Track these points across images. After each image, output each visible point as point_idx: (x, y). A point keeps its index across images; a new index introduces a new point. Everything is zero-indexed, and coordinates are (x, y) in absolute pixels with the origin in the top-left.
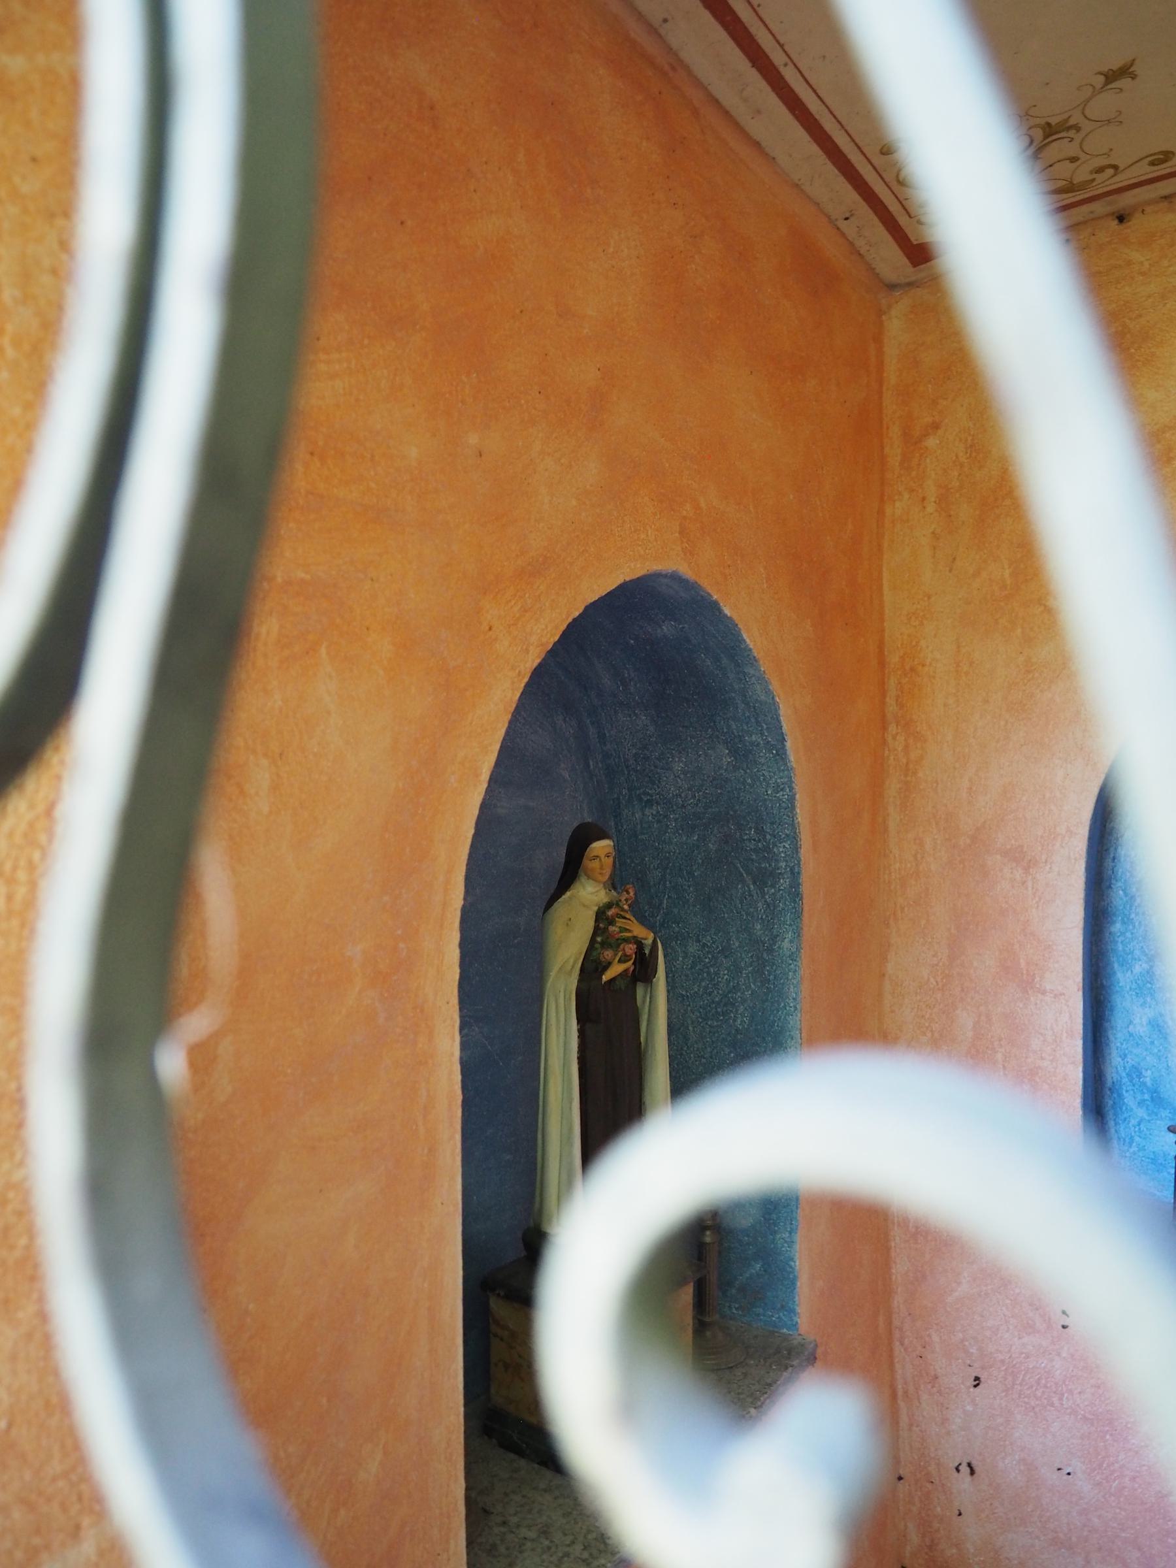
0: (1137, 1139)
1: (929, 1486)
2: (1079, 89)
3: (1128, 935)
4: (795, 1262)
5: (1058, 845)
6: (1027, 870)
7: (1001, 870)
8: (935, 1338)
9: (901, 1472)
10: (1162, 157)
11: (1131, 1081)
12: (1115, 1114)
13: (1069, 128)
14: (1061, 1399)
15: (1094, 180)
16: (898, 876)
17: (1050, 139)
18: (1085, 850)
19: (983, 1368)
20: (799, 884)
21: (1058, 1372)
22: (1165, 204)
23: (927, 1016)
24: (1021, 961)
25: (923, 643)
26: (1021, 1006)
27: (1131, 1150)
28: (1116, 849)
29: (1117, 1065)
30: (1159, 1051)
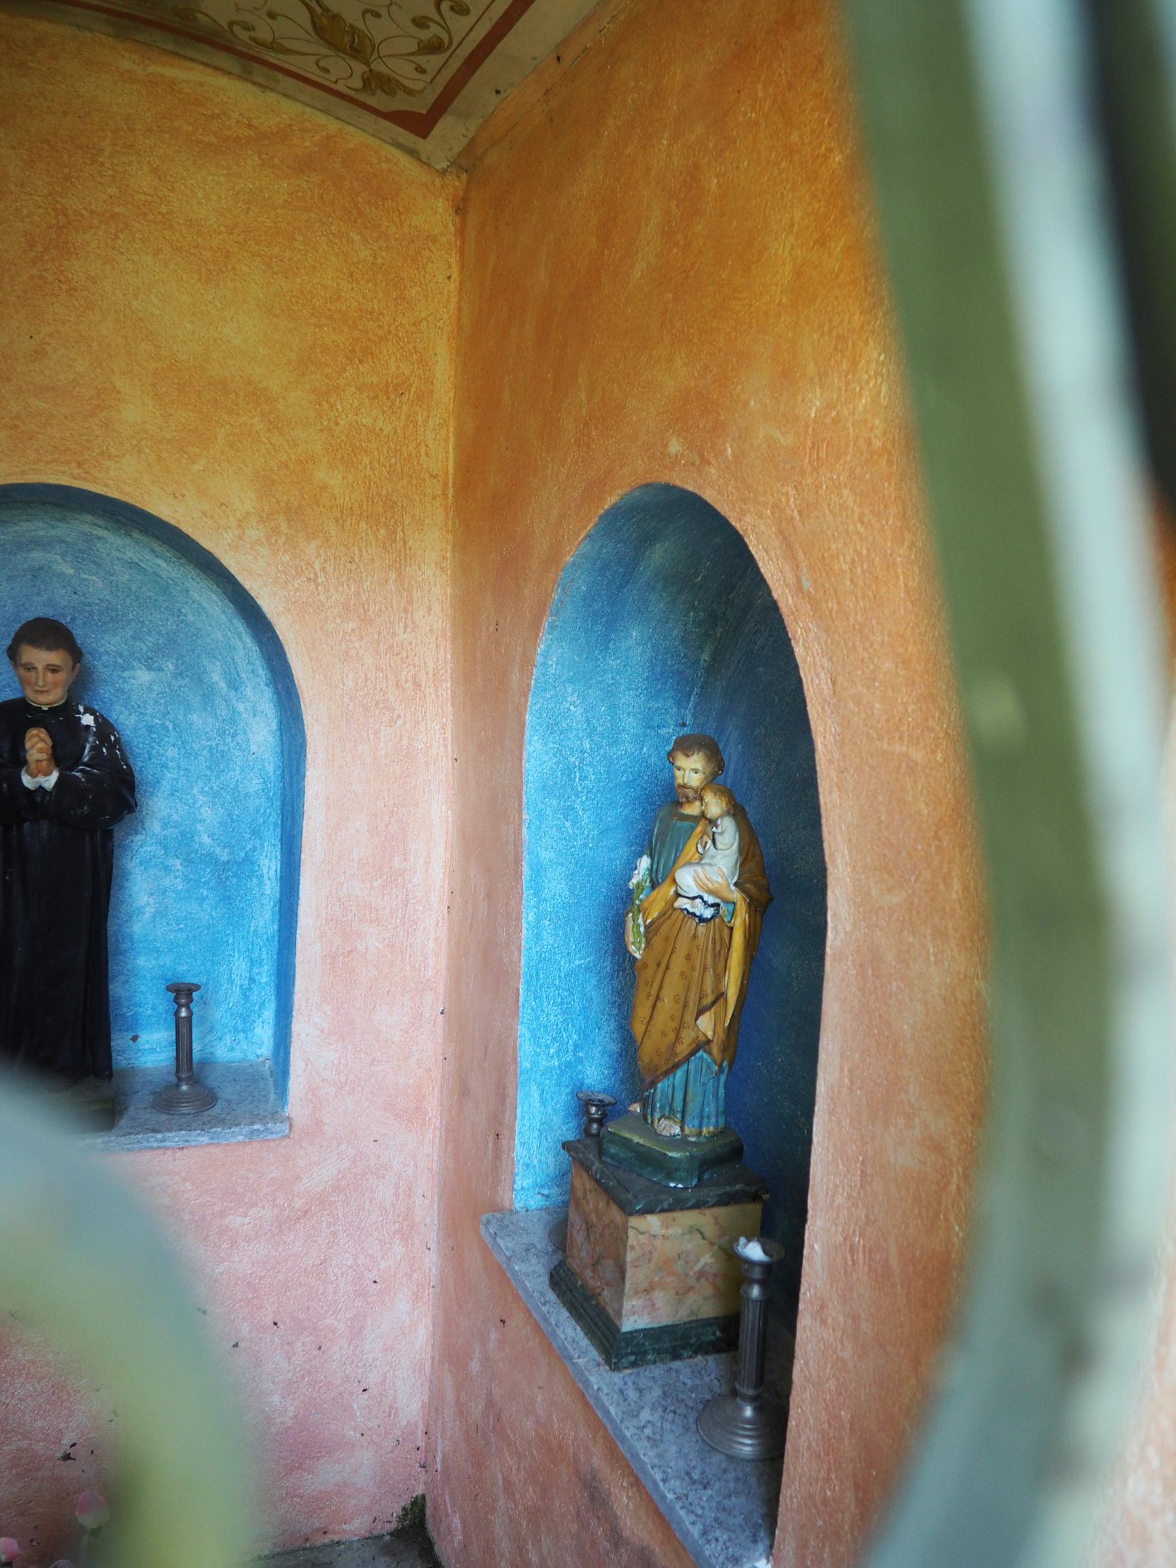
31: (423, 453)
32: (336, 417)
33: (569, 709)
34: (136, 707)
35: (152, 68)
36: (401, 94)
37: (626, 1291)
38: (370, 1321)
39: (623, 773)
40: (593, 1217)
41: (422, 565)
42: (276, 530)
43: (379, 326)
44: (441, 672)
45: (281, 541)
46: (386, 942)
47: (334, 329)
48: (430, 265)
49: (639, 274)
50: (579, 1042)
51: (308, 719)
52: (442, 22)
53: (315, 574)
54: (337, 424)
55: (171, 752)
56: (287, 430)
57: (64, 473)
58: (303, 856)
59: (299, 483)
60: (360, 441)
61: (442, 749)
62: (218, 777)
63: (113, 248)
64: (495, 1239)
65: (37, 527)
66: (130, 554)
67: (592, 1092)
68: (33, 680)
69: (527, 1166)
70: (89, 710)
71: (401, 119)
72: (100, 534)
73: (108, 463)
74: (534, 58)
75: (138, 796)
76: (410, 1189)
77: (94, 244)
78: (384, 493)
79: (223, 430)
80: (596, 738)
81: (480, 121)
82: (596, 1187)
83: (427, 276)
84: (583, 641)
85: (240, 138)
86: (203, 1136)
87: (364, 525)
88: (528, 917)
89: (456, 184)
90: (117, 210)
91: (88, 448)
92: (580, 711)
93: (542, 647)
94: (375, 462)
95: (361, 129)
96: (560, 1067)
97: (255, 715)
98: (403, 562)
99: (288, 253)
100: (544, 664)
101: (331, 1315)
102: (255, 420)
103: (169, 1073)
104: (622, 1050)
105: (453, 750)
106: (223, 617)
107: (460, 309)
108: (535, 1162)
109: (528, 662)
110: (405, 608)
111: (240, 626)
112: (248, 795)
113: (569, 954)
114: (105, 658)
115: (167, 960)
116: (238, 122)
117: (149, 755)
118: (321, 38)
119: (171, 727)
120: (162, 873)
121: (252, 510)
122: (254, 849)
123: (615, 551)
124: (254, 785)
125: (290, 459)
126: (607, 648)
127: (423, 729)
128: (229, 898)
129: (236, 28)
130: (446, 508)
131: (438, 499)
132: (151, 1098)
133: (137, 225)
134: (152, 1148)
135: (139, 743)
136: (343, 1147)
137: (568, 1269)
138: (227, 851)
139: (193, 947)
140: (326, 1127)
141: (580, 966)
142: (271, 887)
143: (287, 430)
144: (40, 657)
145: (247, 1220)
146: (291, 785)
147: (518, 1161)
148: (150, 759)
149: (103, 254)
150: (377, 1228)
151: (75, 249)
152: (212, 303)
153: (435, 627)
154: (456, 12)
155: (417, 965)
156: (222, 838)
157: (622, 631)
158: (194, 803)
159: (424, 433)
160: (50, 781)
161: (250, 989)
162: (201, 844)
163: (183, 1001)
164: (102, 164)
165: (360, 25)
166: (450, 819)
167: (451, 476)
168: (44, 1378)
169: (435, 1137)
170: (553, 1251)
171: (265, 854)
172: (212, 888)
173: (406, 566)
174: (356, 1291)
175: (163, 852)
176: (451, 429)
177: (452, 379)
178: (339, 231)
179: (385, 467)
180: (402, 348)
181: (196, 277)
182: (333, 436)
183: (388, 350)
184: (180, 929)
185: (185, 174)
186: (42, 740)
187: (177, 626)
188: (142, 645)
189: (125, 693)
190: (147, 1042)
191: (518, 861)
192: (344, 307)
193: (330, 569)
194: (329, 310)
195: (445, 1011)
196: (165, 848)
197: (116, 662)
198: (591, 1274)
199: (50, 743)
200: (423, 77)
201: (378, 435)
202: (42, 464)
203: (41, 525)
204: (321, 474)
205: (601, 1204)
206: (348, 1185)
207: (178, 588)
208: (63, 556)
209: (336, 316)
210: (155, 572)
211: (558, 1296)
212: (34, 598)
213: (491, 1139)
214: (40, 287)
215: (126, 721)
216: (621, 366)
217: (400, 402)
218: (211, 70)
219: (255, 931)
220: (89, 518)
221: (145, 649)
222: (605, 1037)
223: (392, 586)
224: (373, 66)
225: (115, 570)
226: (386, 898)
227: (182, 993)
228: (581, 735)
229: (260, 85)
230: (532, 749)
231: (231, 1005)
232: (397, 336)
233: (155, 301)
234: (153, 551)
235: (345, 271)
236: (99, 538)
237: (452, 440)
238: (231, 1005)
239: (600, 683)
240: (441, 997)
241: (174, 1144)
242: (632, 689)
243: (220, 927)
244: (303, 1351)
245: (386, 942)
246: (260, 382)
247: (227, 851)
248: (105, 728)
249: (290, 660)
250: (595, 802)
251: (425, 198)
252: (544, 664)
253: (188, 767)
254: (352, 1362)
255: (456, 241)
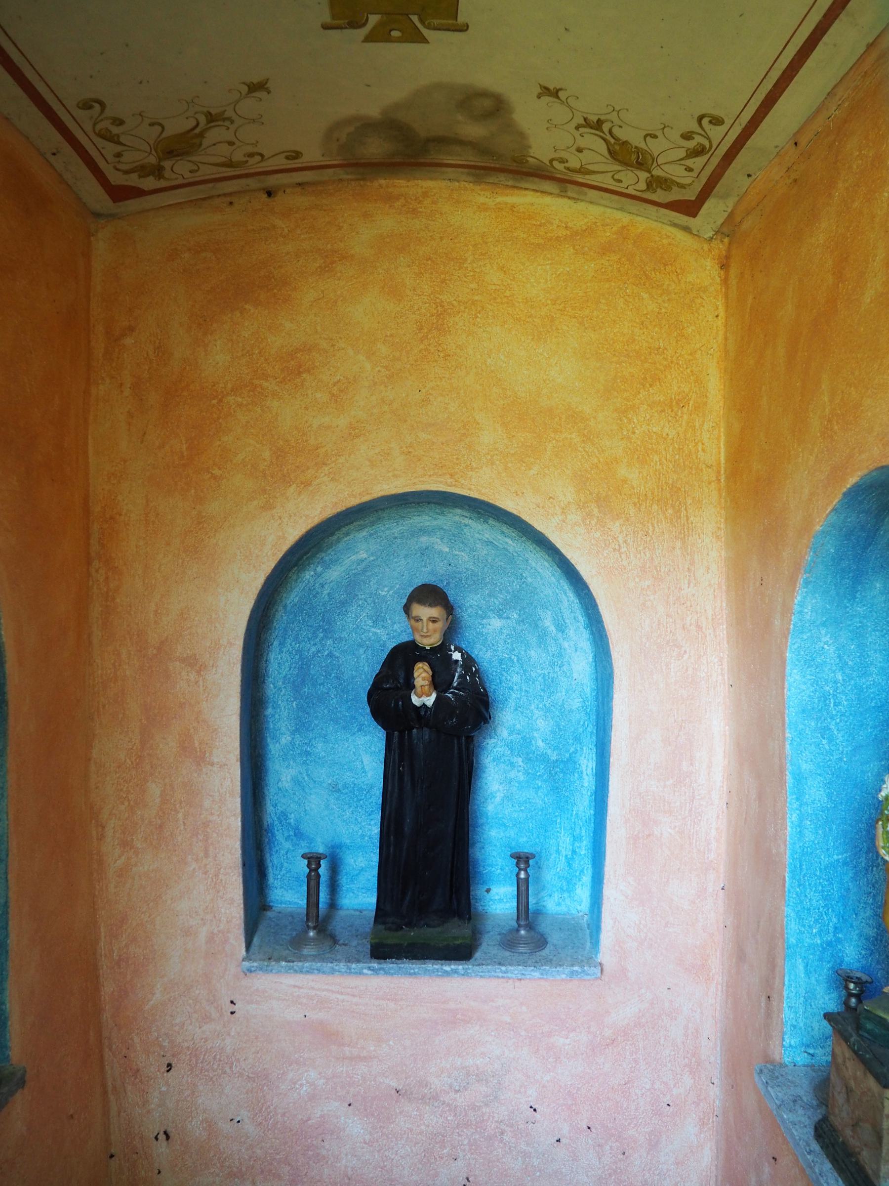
0: (285, 864)
1: (134, 1156)
2: (230, 91)
3: (277, 716)
4: (6, 1005)
5: (221, 653)
6: (199, 672)
7: (180, 673)
8: (136, 1040)
9: (113, 1151)
10: (294, 154)
11: (280, 823)
12: (270, 849)
13: (224, 120)
14: (231, 1068)
15: (247, 162)
16: (100, 681)
17: (212, 124)
18: (240, 656)
19: (174, 1056)
20: (5, 693)
21: (229, 1048)
22: (299, 189)
23: (125, 789)
24: (196, 742)
25: (120, 498)
26: (196, 775)
27: (282, 873)
28: (268, 654)
29: (271, 813)
30: (299, 799)
31: (700, 449)
32: (633, 428)
33: (823, 648)
34: (491, 645)
35: (499, 199)
36: (675, 189)
37: (884, 1154)
38: (664, 1136)
39: (872, 700)
40: (852, 1084)
41: (701, 535)
42: (590, 515)
43: (664, 358)
44: (718, 617)
45: (593, 522)
46: (677, 829)
47: (630, 364)
48: (702, 309)
49: (869, 300)
50: (839, 925)
51: (615, 655)
52: (703, 133)
53: (619, 545)
54: (634, 433)
55: (516, 678)
56: (597, 441)
57: (441, 482)
58: (611, 760)
59: (607, 479)
60: (652, 444)
61: (720, 677)
62: (549, 697)
63: (474, 324)
64: (767, 1087)
65: (424, 519)
66: (487, 536)
67: (851, 970)
68: (420, 628)
69: (795, 1027)
70: (458, 649)
71: (674, 206)
72: (466, 523)
73: (470, 473)
74: (776, 147)
75: (492, 711)
76: (697, 1031)
77: (461, 324)
78: (670, 482)
79: (551, 445)
80: (847, 671)
81: (737, 199)
82: (855, 1057)
83: (700, 317)
84: (833, 593)
85: (560, 237)
86: (536, 971)
87: (656, 507)
88: (792, 817)
89: (720, 247)
90: (476, 298)
91: (457, 464)
92: (832, 649)
93: (799, 598)
94: (663, 460)
95: (646, 217)
96: (822, 945)
97: (576, 650)
98: (686, 533)
99: (595, 313)
100: (801, 612)
101: (634, 1128)
102: (573, 436)
103: (512, 919)
104: (878, 935)
105: (729, 679)
106: (553, 578)
107: (726, 339)
108: (802, 1025)
109: (787, 610)
110: (688, 568)
111: (565, 585)
112: (571, 711)
113: (828, 849)
114: (470, 610)
115: (512, 833)
116: (558, 226)
117: (500, 681)
118: (615, 159)
119: (515, 660)
120: (509, 768)
121: (572, 501)
122: (576, 752)
123: (858, 520)
124: (576, 703)
125: (599, 462)
126: (855, 598)
127: (705, 662)
128: (557, 788)
129: (555, 164)
130: (719, 490)
131: (713, 484)
132: (498, 937)
133: (490, 307)
134: (498, 977)
135: (493, 672)
136: (643, 991)
137: (831, 1125)
138: (555, 753)
139: (531, 824)
140: (630, 974)
141: (838, 860)
142: (588, 781)
143: (597, 441)
144: (424, 612)
145: (568, 1041)
146: (603, 704)
147: (787, 1022)
148: (501, 684)
149: (467, 329)
150: (670, 1061)
151: (449, 328)
152: (541, 355)
153: (712, 582)
154: (715, 124)
155: (702, 849)
156: (552, 742)
157: (867, 583)
158: (532, 717)
159: (701, 434)
160: (430, 700)
161: (573, 859)
162: (537, 747)
163: (522, 866)
164: (467, 268)
165: (642, 145)
166: (727, 733)
167: (723, 466)
168: (418, 1143)
169: (717, 990)
170: (817, 1105)
171: (584, 755)
172: (544, 780)
173: (688, 537)
174: (653, 1110)
175: (509, 752)
176: (722, 430)
177: (722, 392)
178: (633, 293)
179: (671, 462)
180: (682, 372)
181: (530, 337)
182: (631, 442)
183: (671, 375)
184: (521, 810)
185: (522, 267)
186: (425, 671)
187: (520, 586)
188: (495, 600)
189: (483, 635)
190: (497, 894)
191: (782, 771)
192: (637, 347)
193: (630, 542)
194: (626, 350)
195: (726, 888)
196: (511, 749)
197: (477, 613)
198: (851, 1133)
199: (431, 673)
200: (690, 174)
201: (665, 439)
202: (427, 477)
203: (427, 518)
204: (622, 471)
205: (858, 1073)
206: (647, 1022)
207: (521, 558)
208: (442, 539)
209: (631, 354)
210: (504, 548)
211: (822, 1147)
212: (422, 569)
213: (763, 1000)
214: (425, 356)
215: (484, 656)
216: (857, 373)
217: (682, 413)
218: (539, 194)
219: (577, 814)
220: (458, 511)
221: (497, 603)
222: (862, 922)
223: (678, 552)
224: (654, 173)
225: (477, 547)
226: (677, 794)
227: (522, 860)
228: (834, 668)
229: (574, 198)
230: (792, 680)
231: (558, 870)
232: (678, 364)
233: (502, 357)
234: (503, 533)
235: (637, 320)
236: (466, 525)
237: (723, 438)
238: (558, 870)
239: (849, 625)
240: (722, 876)
241: (514, 976)
242: (878, 630)
243: (550, 810)
244: (610, 1153)
245: (677, 829)
246: (576, 408)
247: (555, 753)
248: (469, 661)
249: (601, 610)
250: (848, 723)
251: (696, 260)
252: (801, 612)
253: (528, 689)
254: (650, 1169)
255: (721, 289)
